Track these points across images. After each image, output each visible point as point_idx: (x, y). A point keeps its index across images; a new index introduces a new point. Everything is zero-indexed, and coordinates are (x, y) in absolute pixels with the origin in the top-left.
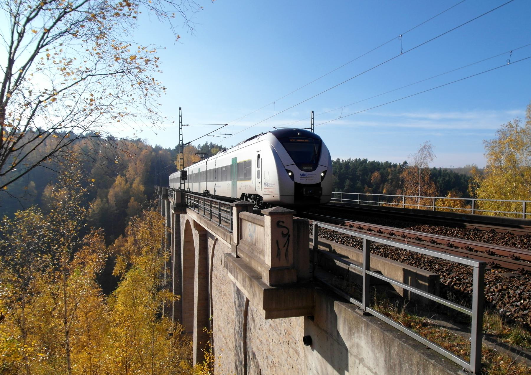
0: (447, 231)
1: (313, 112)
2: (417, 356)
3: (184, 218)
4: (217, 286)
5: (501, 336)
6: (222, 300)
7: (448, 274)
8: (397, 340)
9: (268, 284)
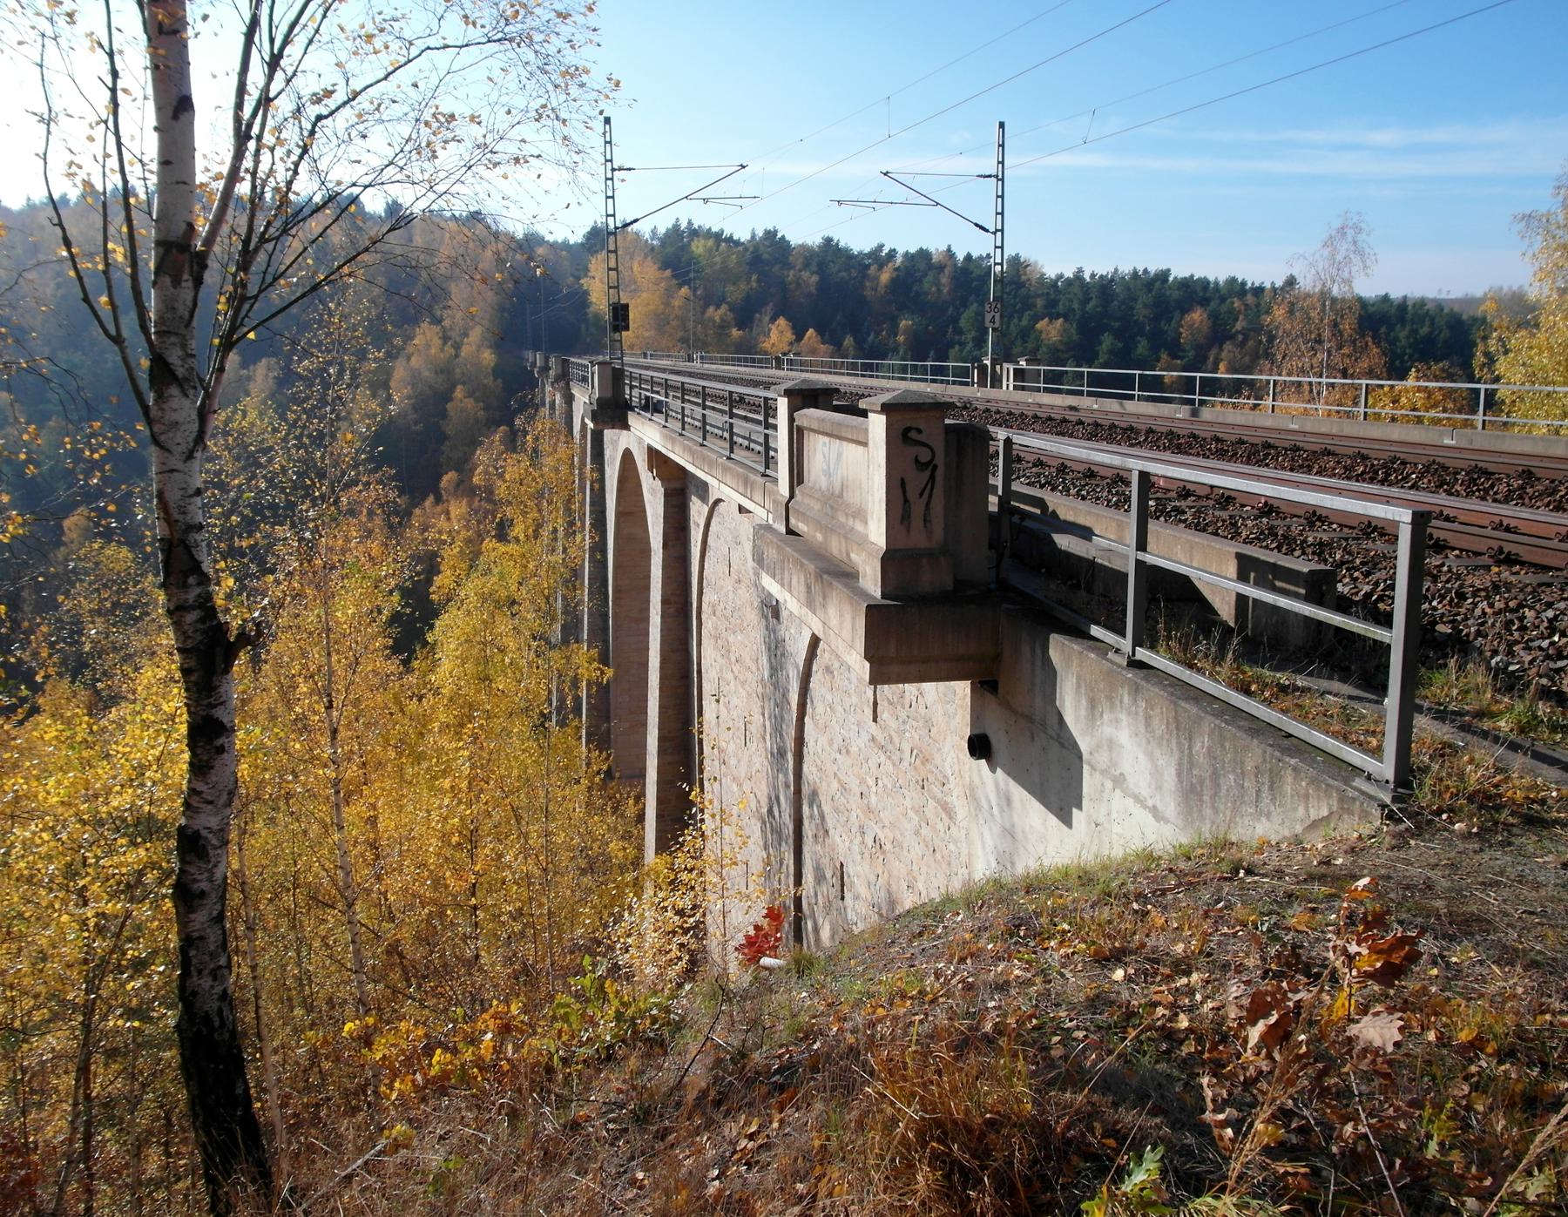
0: (1387, 475)
1: (1002, 125)
2: (1256, 753)
3: (615, 443)
4: (717, 638)
5: (1481, 714)
6: (730, 676)
7: (1367, 575)
8: (1209, 717)
9: (878, 594)
